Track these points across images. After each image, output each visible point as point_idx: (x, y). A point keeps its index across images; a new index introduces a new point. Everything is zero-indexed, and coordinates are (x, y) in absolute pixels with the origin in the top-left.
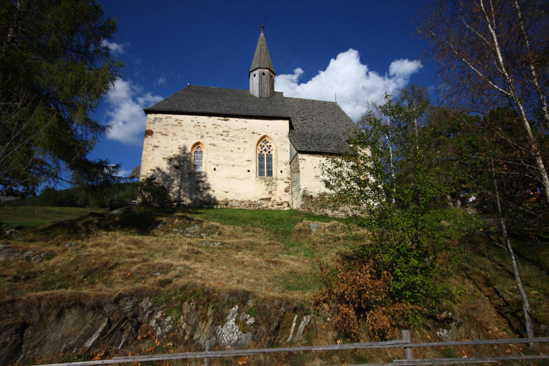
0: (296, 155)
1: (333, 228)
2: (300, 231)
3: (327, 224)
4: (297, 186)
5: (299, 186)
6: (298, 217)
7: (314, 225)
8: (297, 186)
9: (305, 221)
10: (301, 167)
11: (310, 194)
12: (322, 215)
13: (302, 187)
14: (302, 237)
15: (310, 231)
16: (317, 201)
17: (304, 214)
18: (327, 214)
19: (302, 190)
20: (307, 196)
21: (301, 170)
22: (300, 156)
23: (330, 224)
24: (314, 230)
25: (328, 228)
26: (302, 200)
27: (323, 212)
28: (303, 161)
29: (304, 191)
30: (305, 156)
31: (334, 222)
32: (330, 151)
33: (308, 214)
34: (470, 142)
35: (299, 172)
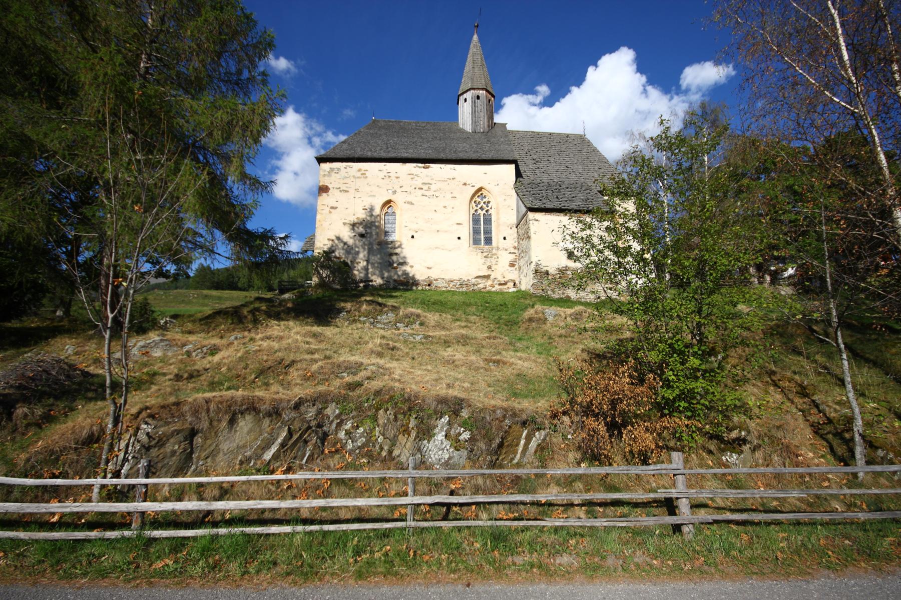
0: (525, 214)
2: (531, 320)
3: (569, 311)
4: (527, 258)
8: (527, 258)
11: (545, 269)
13: (534, 259)
15: (545, 320)
17: (536, 297)
19: (534, 263)
22: (531, 215)
24: (551, 319)
30: (538, 216)
35: (529, 237)
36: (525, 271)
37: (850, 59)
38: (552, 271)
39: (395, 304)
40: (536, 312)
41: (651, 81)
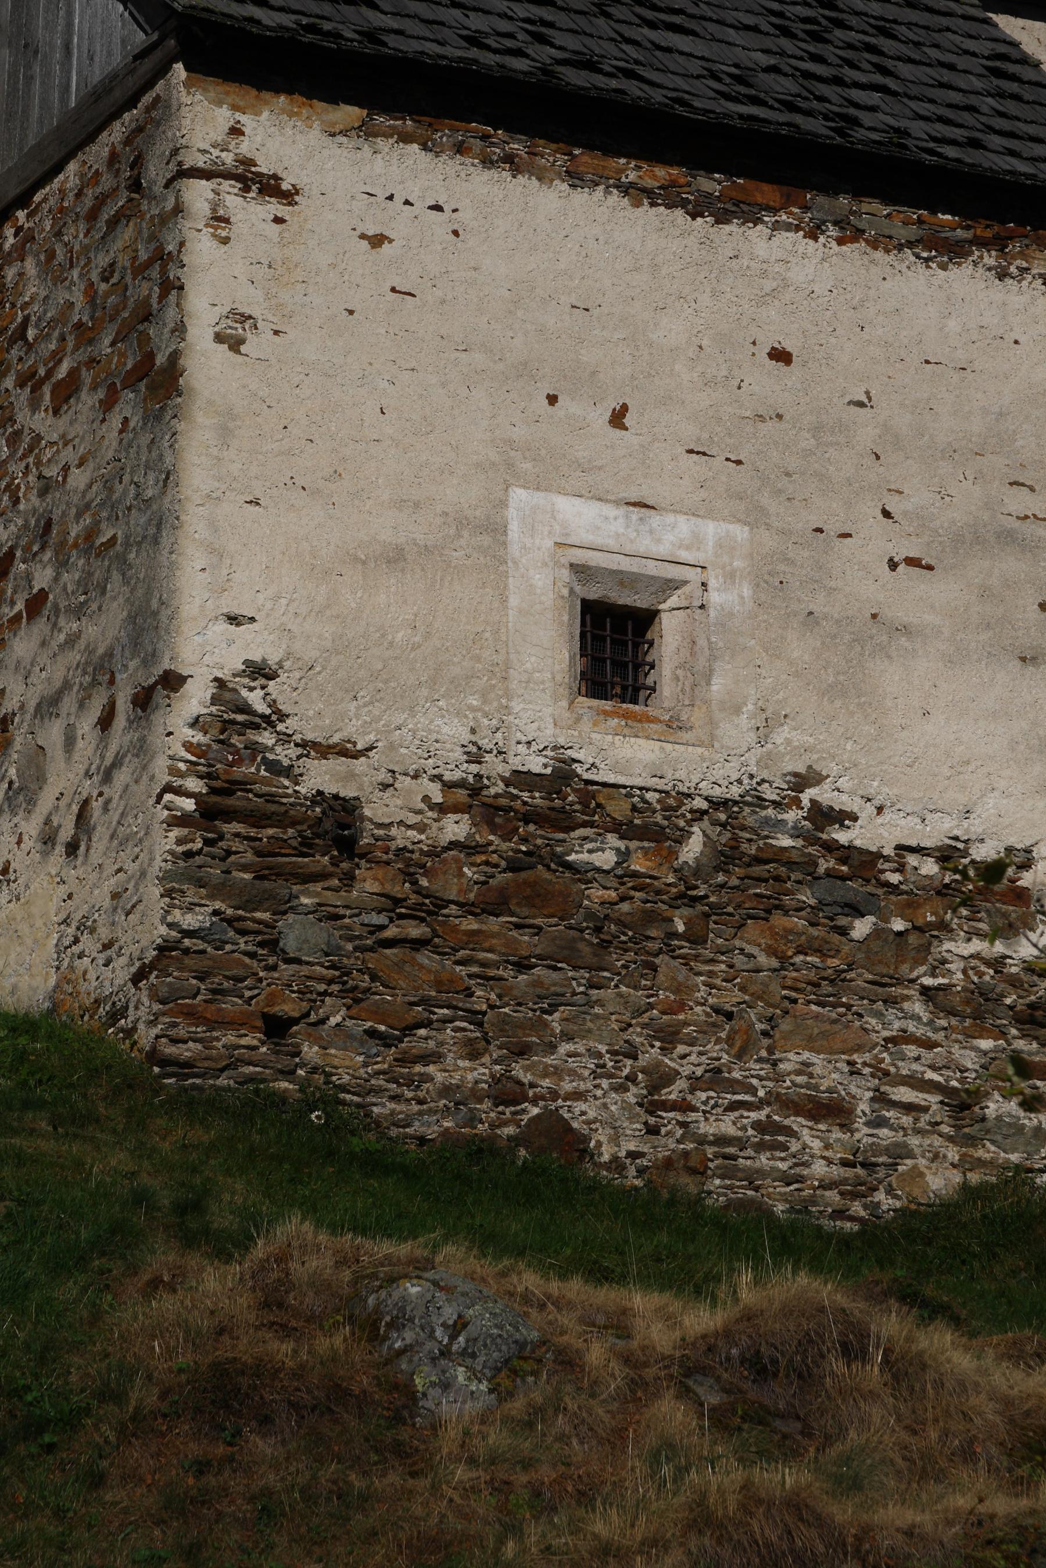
0: (128, 92)
1: (778, 1395)
2: (225, 1396)
3: (665, 1320)
4: (104, 627)
5: (148, 623)
6: (110, 1162)
7: (452, 1301)
8: (104, 627)
9: (308, 1246)
10: (203, 307)
11: (320, 777)
12: (483, 1150)
13: (205, 651)
14: (268, 1509)
15: (388, 1420)
16: (430, 908)
17: (193, 1106)
18: (563, 1140)
19: (195, 699)
20: (269, 813)
21: (206, 365)
22: (203, 118)
23: (701, 1320)
24: (458, 1399)
25: (691, 1367)
26: (184, 876)
27: (507, 1093)
28: (250, 214)
29: (234, 718)
30: (282, 135)
31: (759, 1292)
32: (705, 99)
33: (258, 1105)
34: (99, 362)
35: (159, 382)
36: (64, 779)
37: (953, 215)
38: (390, 811)
39: (419, 1253)
40: (274, 1301)
41: (259, 90)
